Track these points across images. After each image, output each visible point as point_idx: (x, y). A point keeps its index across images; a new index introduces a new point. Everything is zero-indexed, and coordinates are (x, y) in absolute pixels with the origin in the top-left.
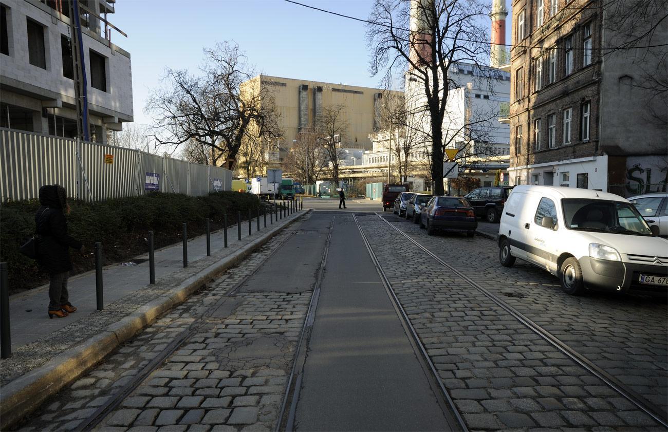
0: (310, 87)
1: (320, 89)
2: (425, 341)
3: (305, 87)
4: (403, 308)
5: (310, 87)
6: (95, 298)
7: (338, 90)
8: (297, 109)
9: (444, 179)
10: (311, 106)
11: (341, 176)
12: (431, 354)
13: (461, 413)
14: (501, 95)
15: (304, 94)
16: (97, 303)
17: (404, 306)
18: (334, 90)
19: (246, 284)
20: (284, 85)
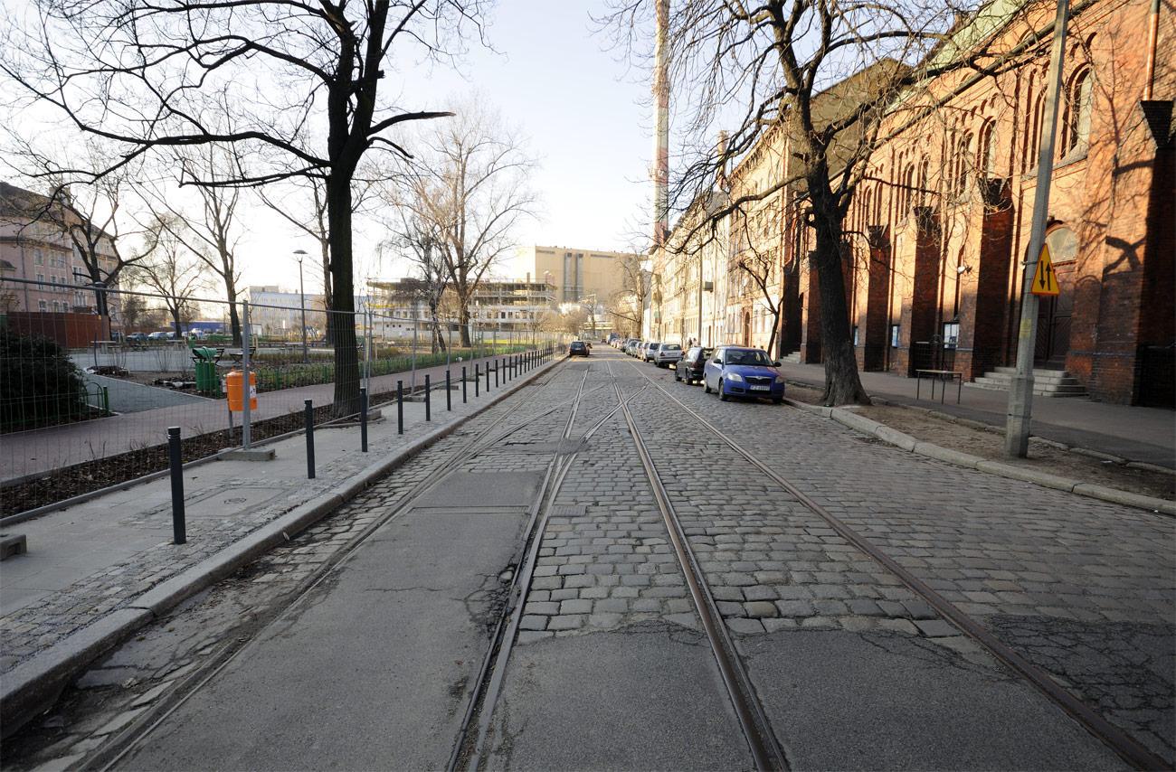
0: (574, 254)
1: (581, 256)
2: (677, 509)
3: (570, 255)
4: (679, 521)
5: (574, 254)
6: (361, 440)
7: (595, 256)
8: (562, 272)
9: (947, 328)
10: (574, 269)
11: (597, 328)
12: (724, 612)
13: (704, 574)
14: (157, 647)
15: (569, 260)
16: (1048, 201)
17: (680, 518)
18: (592, 255)
19: (988, 13)
20: (553, 253)
